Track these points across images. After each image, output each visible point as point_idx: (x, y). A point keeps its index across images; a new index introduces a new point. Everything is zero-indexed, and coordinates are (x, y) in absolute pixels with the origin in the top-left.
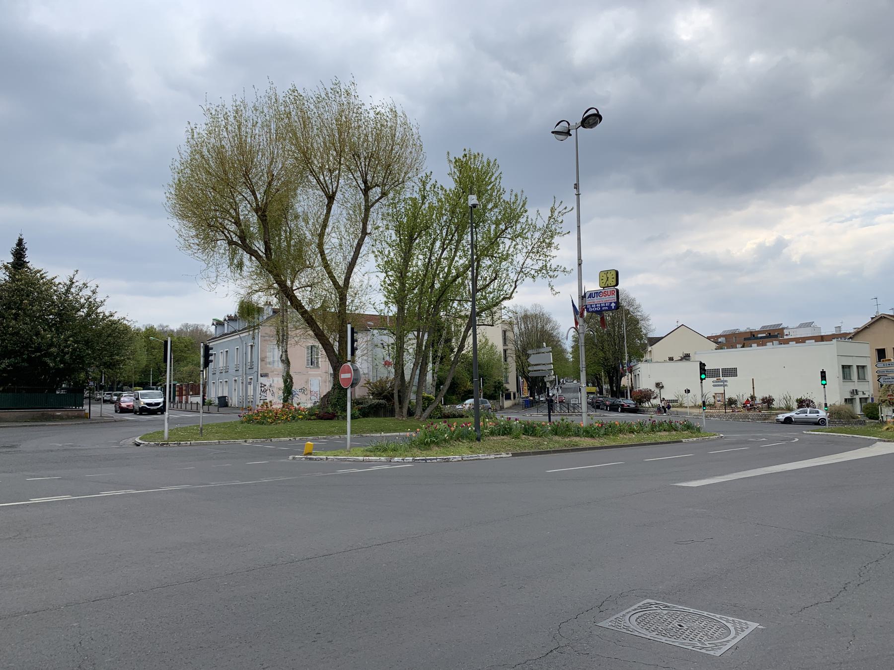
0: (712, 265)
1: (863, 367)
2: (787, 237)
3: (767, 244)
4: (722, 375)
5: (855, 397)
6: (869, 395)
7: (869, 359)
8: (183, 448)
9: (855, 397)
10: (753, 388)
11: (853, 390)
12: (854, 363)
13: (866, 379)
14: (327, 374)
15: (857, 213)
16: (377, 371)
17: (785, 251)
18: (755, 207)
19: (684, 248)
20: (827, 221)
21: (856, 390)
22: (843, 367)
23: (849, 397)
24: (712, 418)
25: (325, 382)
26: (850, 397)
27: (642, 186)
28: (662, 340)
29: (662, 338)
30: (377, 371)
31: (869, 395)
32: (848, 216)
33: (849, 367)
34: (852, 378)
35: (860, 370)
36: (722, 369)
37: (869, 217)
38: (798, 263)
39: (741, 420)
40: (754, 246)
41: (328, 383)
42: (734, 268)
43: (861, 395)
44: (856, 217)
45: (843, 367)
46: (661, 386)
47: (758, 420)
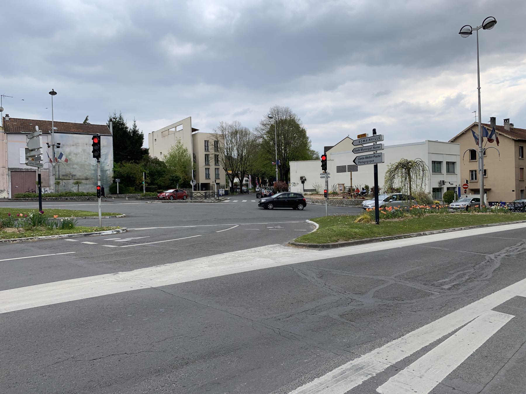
0: (416, 110)
1: (454, 163)
2: (464, 93)
3: (452, 98)
4: (348, 170)
5: (443, 186)
6: (456, 186)
7: (459, 156)
8: (117, 218)
9: (443, 186)
10: (351, 179)
11: (441, 181)
12: (445, 159)
13: (455, 172)
14: (4, 168)
15: (507, 78)
16: (59, 167)
17: (462, 101)
18: (445, 75)
19: (401, 100)
20: (489, 83)
21: (443, 181)
22: (434, 162)
23: (437, 186)
24: (317, 204)
25: (3, 175)
26: (438, 187)
27: (372, 62)
28: (333, 148)
29: (333, 146)
30: (59, 167)
31: (456, 186)
32: (502, 80)
33: (440, 163)
34: (442, 172)
35: (451, 166)
36: (348, 166)
37: (515, 80)
38: (470, 109)
39: (337, 205)
40: (444, 99)
41: (5, 176)
42: (428, 111)
43: (447, 185)
44: (507, 80)
45: (434, 162)
46: (304, 179)
47: (351, 205)
